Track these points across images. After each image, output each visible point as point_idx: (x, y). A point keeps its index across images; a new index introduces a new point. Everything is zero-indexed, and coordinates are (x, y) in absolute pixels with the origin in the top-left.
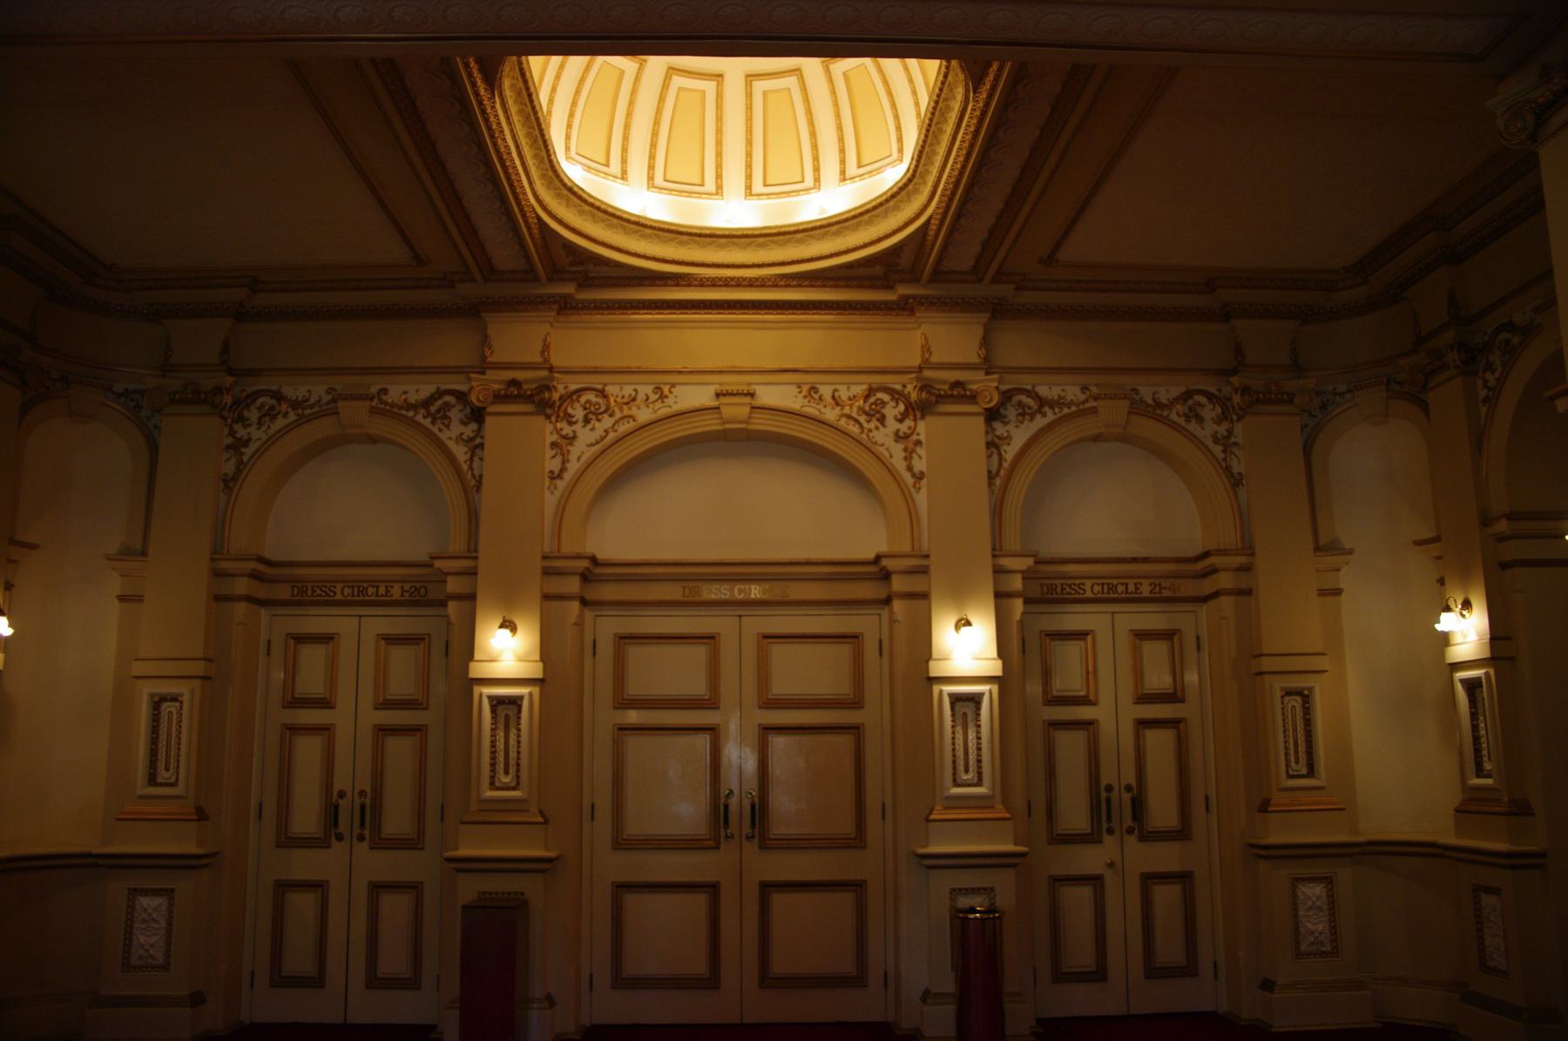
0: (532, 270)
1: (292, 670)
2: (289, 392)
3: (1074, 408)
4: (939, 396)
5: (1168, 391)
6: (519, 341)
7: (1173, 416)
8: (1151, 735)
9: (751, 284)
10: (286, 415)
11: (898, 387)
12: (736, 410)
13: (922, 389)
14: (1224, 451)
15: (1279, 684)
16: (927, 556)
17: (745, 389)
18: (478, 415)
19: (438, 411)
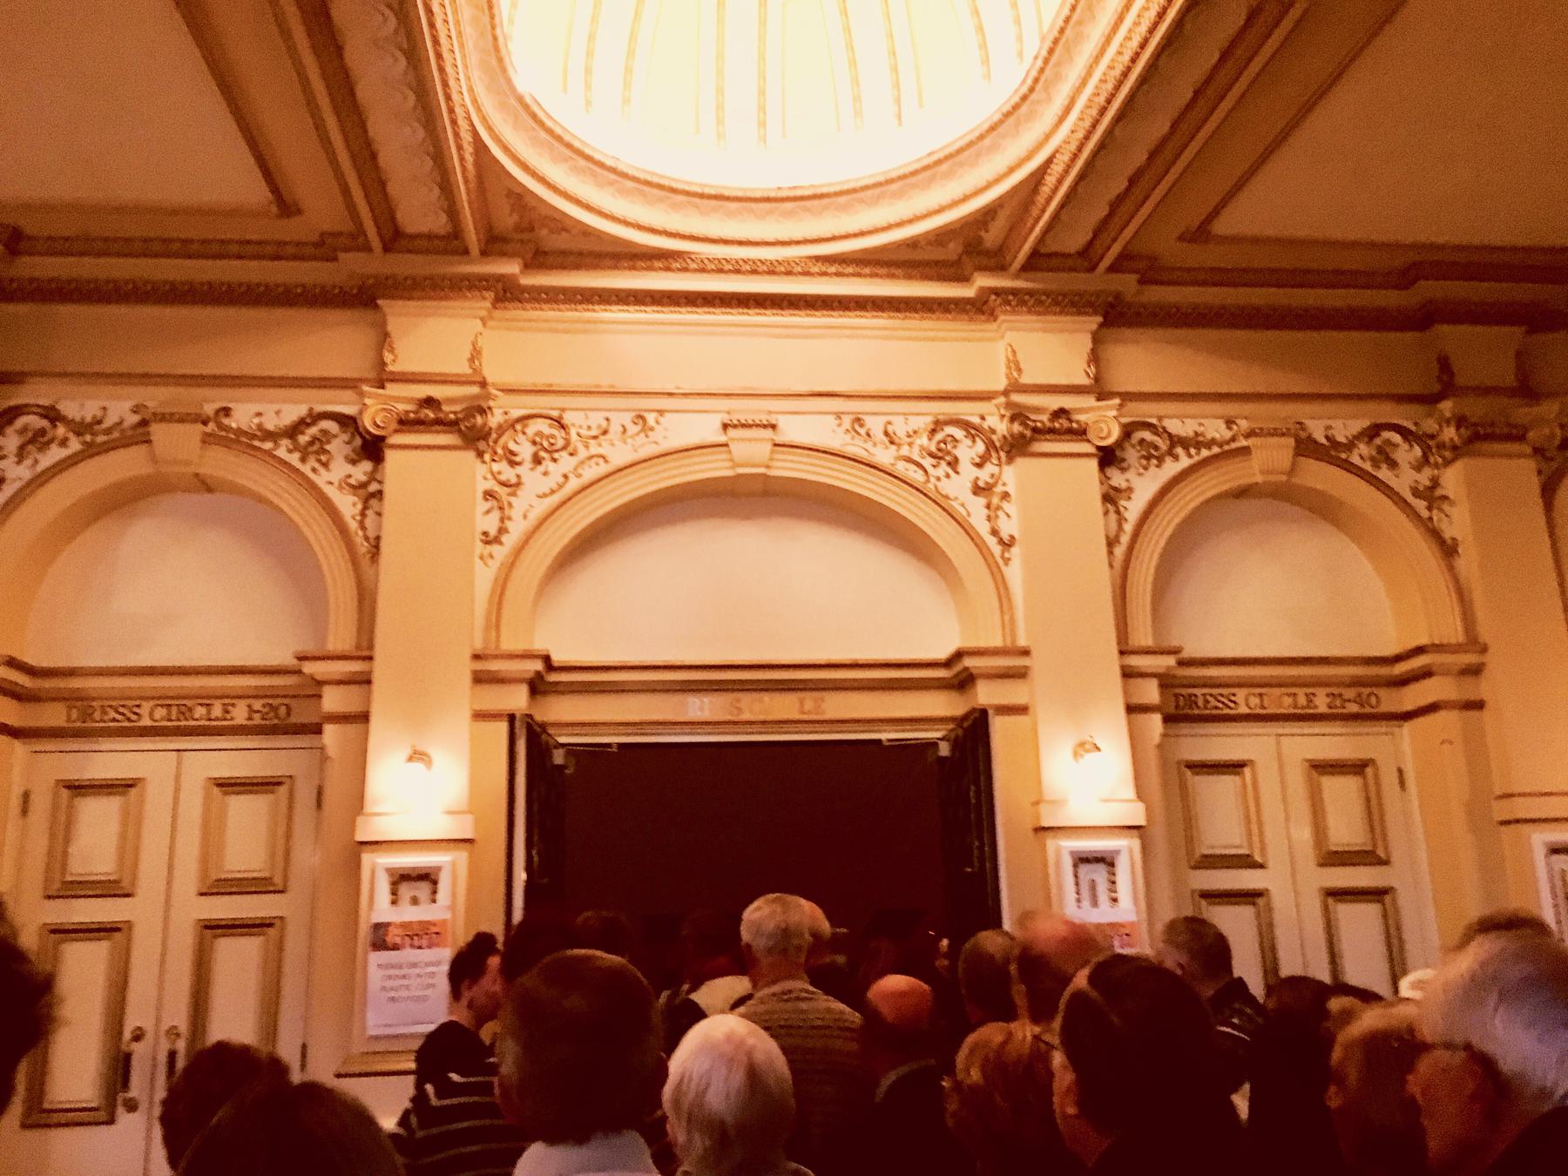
0: (456, 234)
1: (62, 832)
2: (70, 409)
3: (1216, 450)
4: (1035, 430)
5: (1345, 424)
6: (437, 341)
7: (1355, 459)
8: (1346, 912)
9: (772, 270)
10: (64, 443)
11: (976, 420)
12: (751, 453)
13: (1013, 419)
14: (1430, 508)
15: (1540, 838)
16: (1026, 652)
17: (764, 419)
18: (372, 449)
19: (311, 443)
